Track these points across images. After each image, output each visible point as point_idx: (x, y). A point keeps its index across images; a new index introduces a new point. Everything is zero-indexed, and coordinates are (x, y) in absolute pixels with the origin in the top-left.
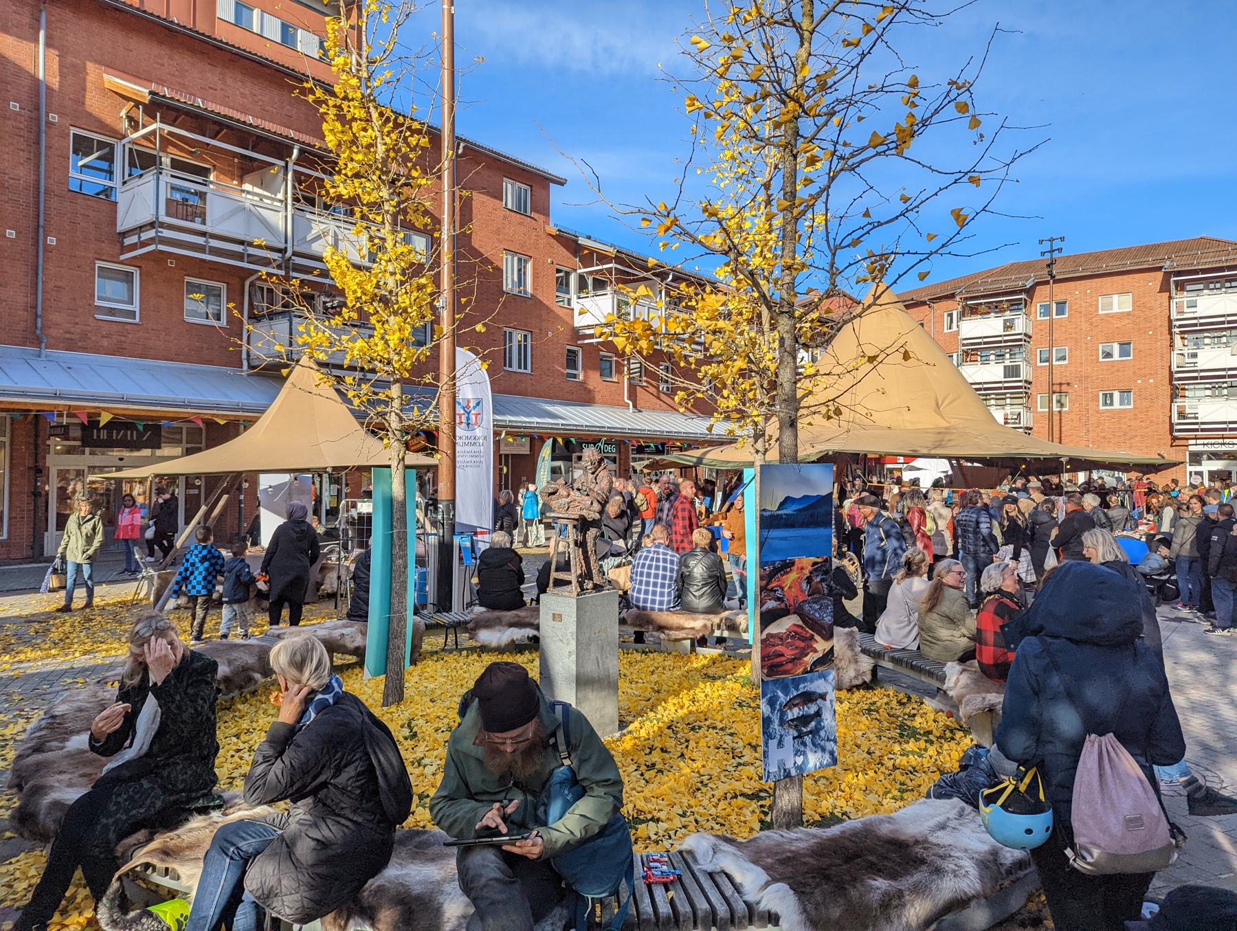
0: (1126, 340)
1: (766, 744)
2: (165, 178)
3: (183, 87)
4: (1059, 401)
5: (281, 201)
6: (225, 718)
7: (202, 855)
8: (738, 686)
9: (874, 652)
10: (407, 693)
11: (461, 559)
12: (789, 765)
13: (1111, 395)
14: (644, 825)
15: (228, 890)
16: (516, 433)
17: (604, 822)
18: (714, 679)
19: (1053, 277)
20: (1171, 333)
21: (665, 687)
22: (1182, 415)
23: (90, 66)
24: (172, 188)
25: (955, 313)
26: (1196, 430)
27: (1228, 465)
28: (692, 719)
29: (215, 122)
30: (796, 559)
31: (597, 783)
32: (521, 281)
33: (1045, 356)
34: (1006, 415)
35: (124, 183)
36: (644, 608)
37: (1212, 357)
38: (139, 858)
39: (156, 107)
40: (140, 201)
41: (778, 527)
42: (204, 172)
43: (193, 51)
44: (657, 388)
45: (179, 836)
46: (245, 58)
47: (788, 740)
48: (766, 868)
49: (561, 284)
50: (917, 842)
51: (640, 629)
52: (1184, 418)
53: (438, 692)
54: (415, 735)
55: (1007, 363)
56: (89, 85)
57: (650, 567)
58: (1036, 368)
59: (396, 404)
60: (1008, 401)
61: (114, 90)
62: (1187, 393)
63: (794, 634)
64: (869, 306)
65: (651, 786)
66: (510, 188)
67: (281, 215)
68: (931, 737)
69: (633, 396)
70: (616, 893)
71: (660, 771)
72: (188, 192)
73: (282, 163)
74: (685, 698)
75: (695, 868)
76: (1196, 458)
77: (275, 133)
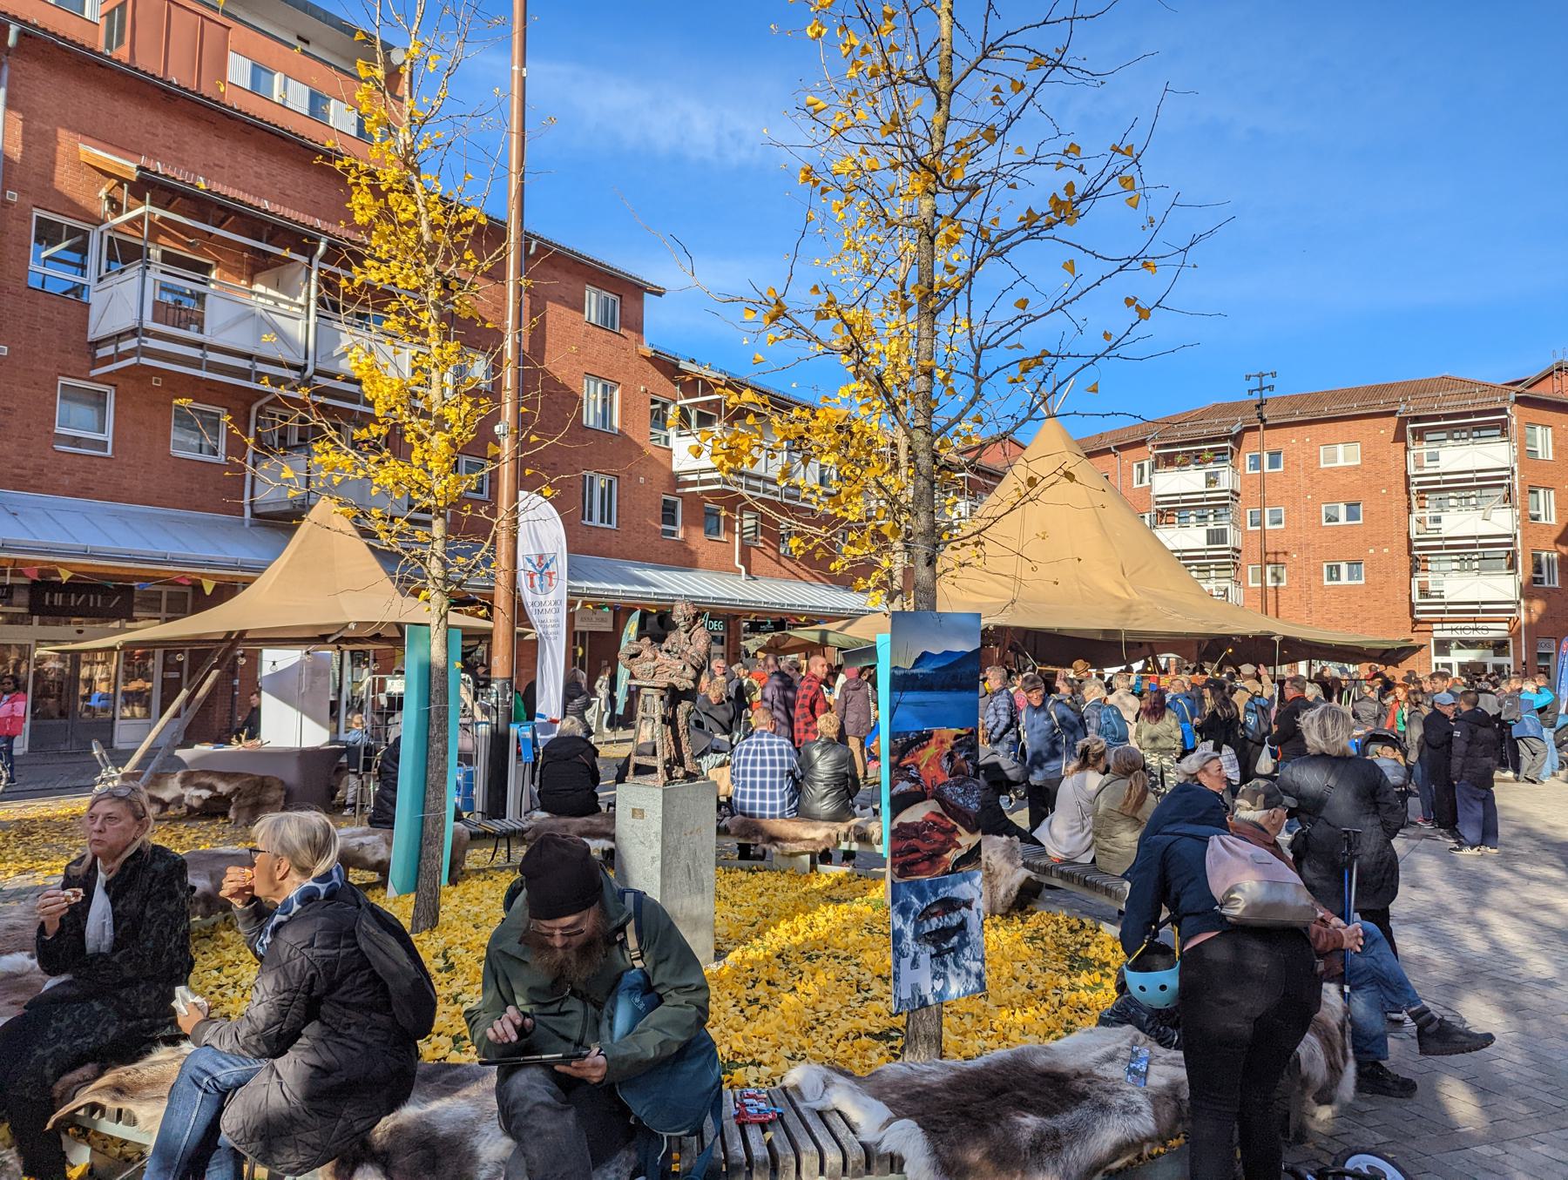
0: (1354, 500)
1: (897, 964)
2: (154, 275)
4: (1274, 574)
5: (301, 306)
6: (205, 949)
7: (165, 1094)
8: (868, 909)
10: (442, 918)
11: (519, 753)
12: (926, 990)
13: (1338, 568)
14: (741, 1070)
15: (200, 1131)
16: (598, 604)
18: (839, 902)
19: (1263, 421)
20: (1408, 492)
21: (776, 911)
24: (162, 289)
25: (1146, 464)
26: (1442, 612)
28: (807, 948)
29: (221, 207)
30: (935, 730)
31: (676, 988)
32: (606, 416)
33: (1257, 518)
35: (100, 280)
36: (752, 816)
38: (85, 1097)
39: (144, 186)
40: (120, 303)
42: (205, 269)
44: (777, 551)
45: (137, 1071)
46: (263, 129)
47: (924, 959)
48: (890, 1105)
49: (657, 418)
50: (1079, 1075)
51: (747, 842)
52: (1427, 596)
53: (485, 916)
54: (452, 966)
55: (1211, 526)
56: (60, 157)
57: (754, 763)
58: (1245, 533)
59: (439, 546)
60: (1213, 573)
62: (1429, 566)
64: (1024, 421)
65: (751, 1025)
66: (593, 298)
67: (301, 324)
68: (1108, 970)
69: (746, 559)
70: (699, 1132)
71: (766, 1007)
72: (182, 294)
73: (305, 260)
74: (801, 922)
75: (801, 1105)
76: (1443, 647)
77: (296, 222)
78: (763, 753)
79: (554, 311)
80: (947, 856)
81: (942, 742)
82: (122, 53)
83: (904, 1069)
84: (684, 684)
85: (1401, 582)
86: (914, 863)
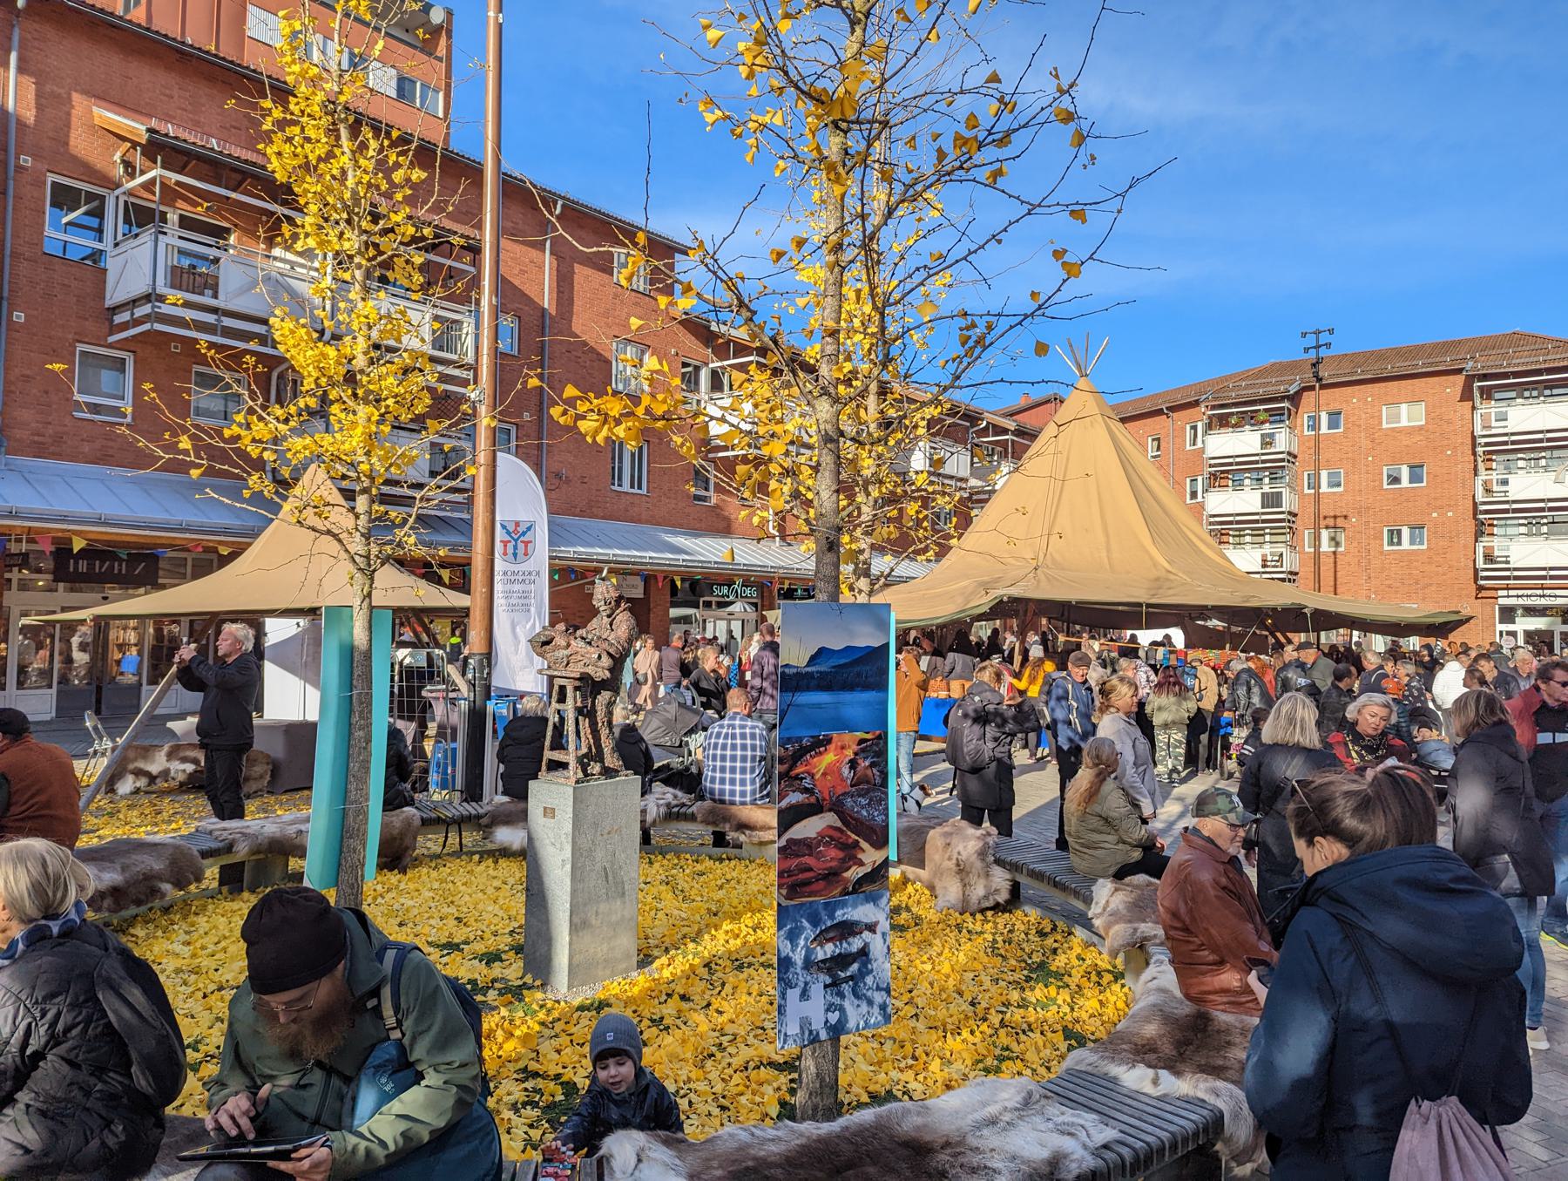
0: (1417, 461)
1: (783, 996)
3: (196, 125)
4: (1333, 539)
9: (1010, 864)
11: (495, 731)
13: (1399, 532)
17: (441, 1123)
20: (1474, 454)
21: (726, 908)
22: (1489, 558)
23: (76, 97)
25: (1200, 425)
26: (1508, 578)
29: (235, 170)
30: (834, 734)
34: (1264, 556)
35: (116, 245)
36: (722, 802)
37: (1528, 484)
39: (156, 148)
40: (135, 267)
42: (220, 233)
47: (817, 990)
52: (1492, 561)
55: (1266, 489)
57: (724, 747)
58: (1302, 496)
60: (1268, 538)
61: (104, 128)
62: (1495, 530)
63: (829, 837)
76: (1508, 614)
78: (734, 737)
79: (581, 273)
80: (847, 875)
81: (843, 748)
83: (744, 1136)
84: (601, 673)
85: (1465, 546)
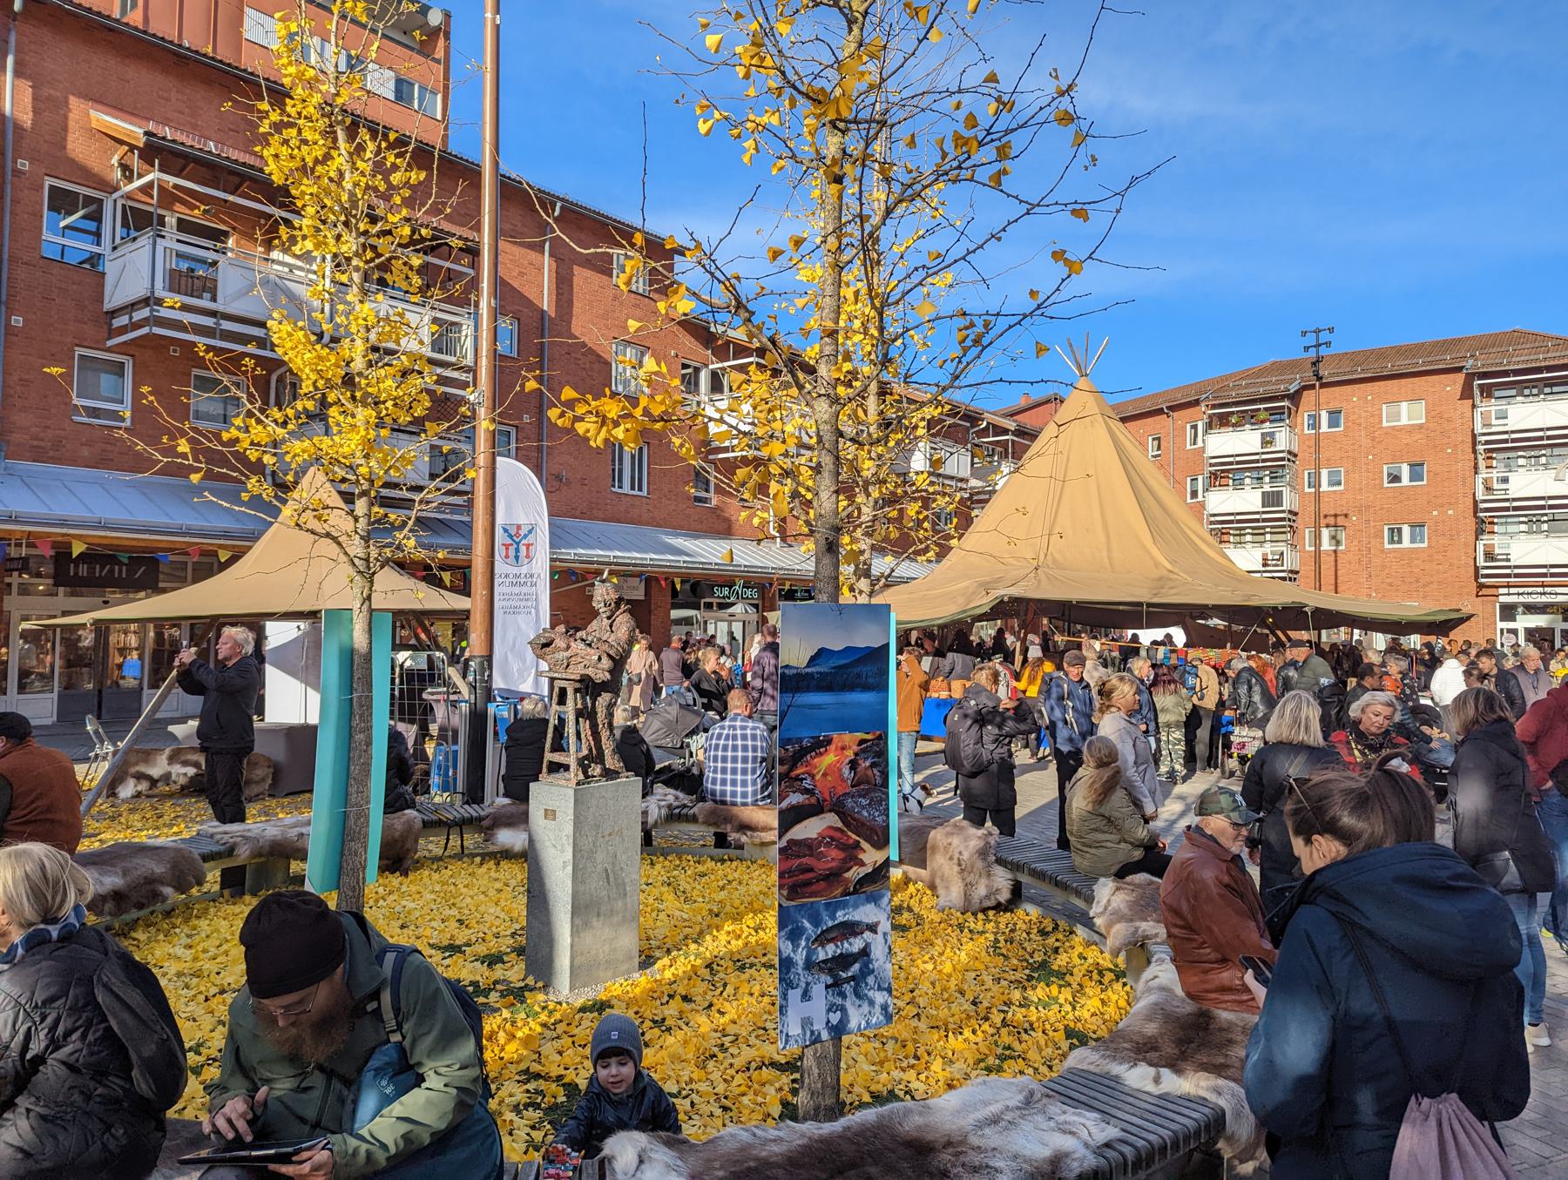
0: (1417, 460)
1: (785, 996)
3: (194, 128)
4: (1333, 537)
9: (1012, 863)
11: (496, 733)
13: (1400, 530)
20: (1475, 451)
22: (1489, 556)
25: (1200, 424)
26: (1508, 576)
27: (1553, 621)
30: (835, 735)
35: (115, 248)
36: (724, 803)
37: (1528, 482)
39: (154, 151)
40: (133, 270)
41: (808, 690)
42: (218, 236)
43: (207, 82)
47: (818, 990)
52: (1493, 559)
55: (1267, 488)
56: (71, 124)
57: (725, 748)
58: (1303, 495)
60: (1268, 537)
61: (102, 132)
62: (1496, 528)
76: (1509, 612)
78: (735, 738)
80: (847, 875)
82: (135, 18)
84: (602, 676)
85: (1466, 545)
86: (808, 884)
